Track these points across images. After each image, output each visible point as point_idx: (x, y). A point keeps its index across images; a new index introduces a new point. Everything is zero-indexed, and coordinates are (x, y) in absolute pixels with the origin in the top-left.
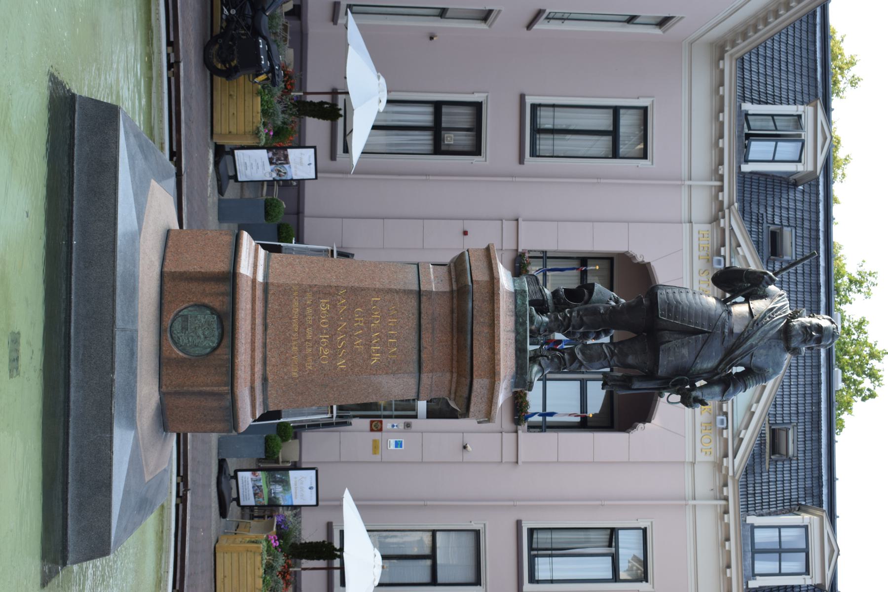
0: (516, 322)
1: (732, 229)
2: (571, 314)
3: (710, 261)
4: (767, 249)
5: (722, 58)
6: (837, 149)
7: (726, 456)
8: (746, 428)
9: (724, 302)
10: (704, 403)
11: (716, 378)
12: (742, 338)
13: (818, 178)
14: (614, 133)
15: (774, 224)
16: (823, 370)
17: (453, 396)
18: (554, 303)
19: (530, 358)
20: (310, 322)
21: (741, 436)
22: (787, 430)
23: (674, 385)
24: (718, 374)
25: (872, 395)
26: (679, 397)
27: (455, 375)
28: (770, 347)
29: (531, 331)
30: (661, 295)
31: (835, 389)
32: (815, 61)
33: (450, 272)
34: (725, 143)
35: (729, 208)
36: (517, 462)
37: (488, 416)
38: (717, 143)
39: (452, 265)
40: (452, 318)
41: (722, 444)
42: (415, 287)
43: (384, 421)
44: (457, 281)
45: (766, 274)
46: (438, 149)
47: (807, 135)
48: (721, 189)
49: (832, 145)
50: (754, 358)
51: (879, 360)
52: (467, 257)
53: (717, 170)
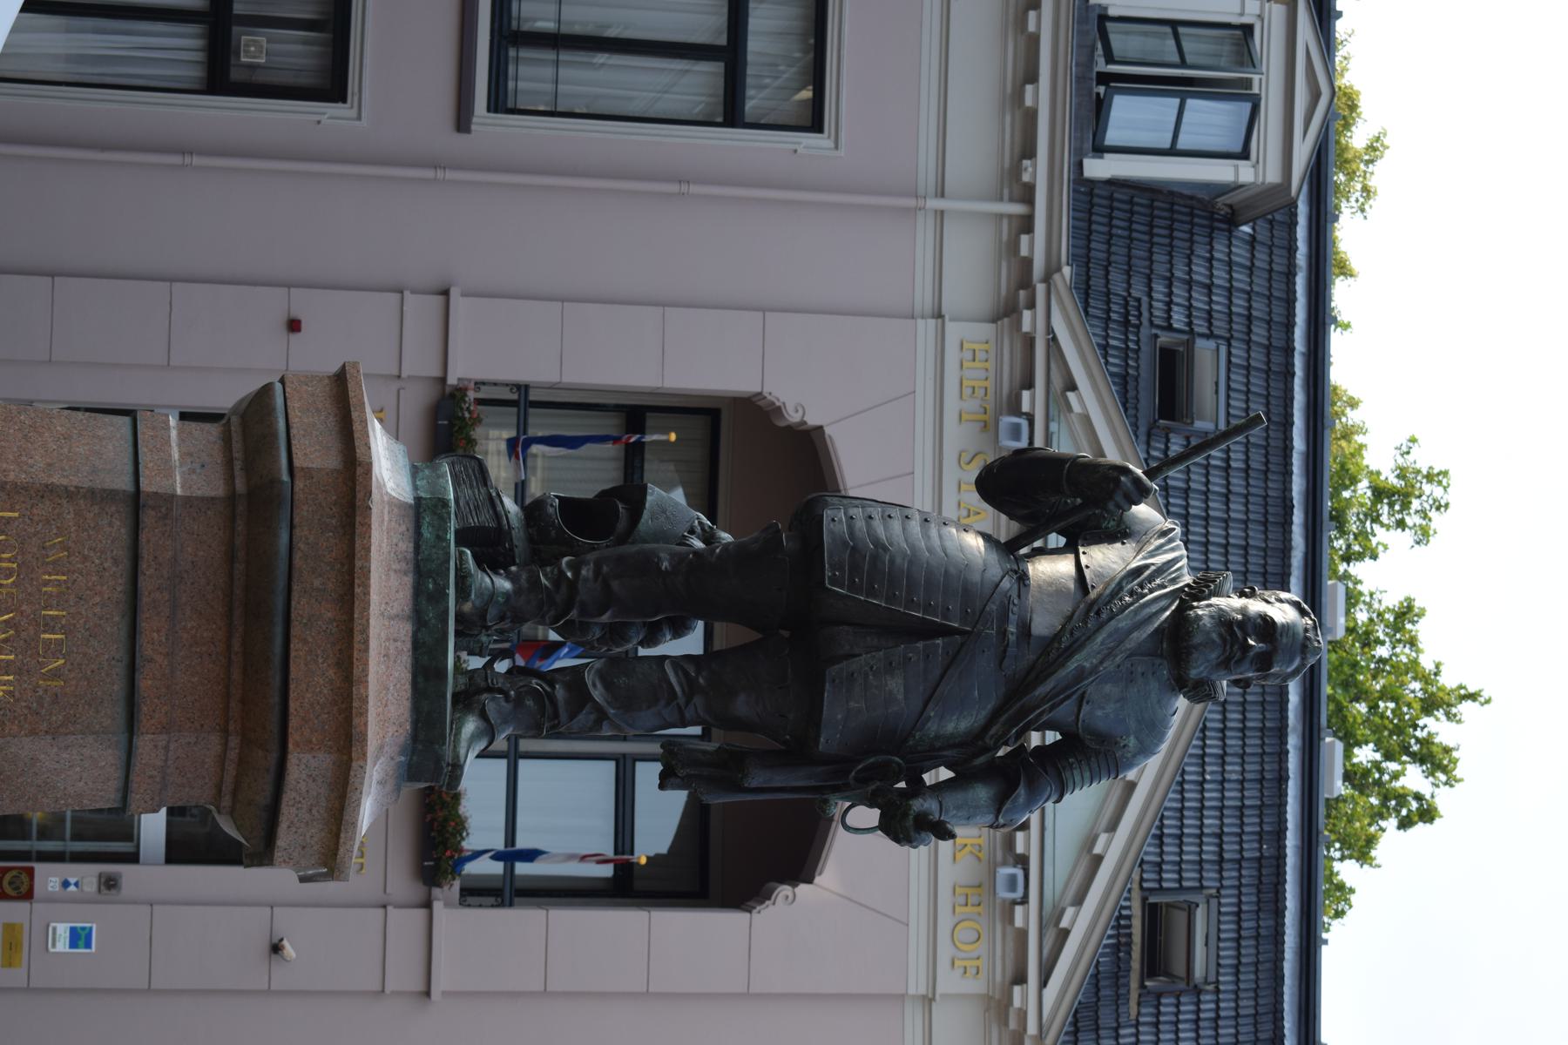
0: (418, 591)
1: (1053, 340)
2: (577, 573)
3: (989, 427)
4: (1148, 398)
6: (1347, 126)
7: (1020, 979)
8: (1079, 901)
9: (1008, 549)
10: (944, 833)
11: (981, 760)
12: (1057, 648)
13: (1293, 205)
14: (730, 53)
15: (1170, 328)
16: (1293, 742)
17: (226, 801)
18: (530, 540)
19: (455, 695)
21: (1064, 924)
22: (1190, 909)
23: (863, 780)
24: (986, 750)
25: (1428, 814)
26: (876, 812)
27: (234, 741)
28: (1130, 678)
29: (459, 617)
30: (834, 521)
31: (1325, 794)
33: (227, 439)
34: (1041, 96)
35: (1047, 279)
36: (428, 994)
37: (329, 860)
38: (1019, 95)
39: (235, 420)
40: (231, 576)
41: (1010, 945)
42: (124, 483)
43: (40, 868)
44: (249, 468)
45: (1126, 471)
46: (220, 76)
47: (1268, 82)
48: (1026, 224)
49: (1338, 110)
50: (1086, 708)
51: (1450, 717)
52: (279, 401)
53: (1016, 171)
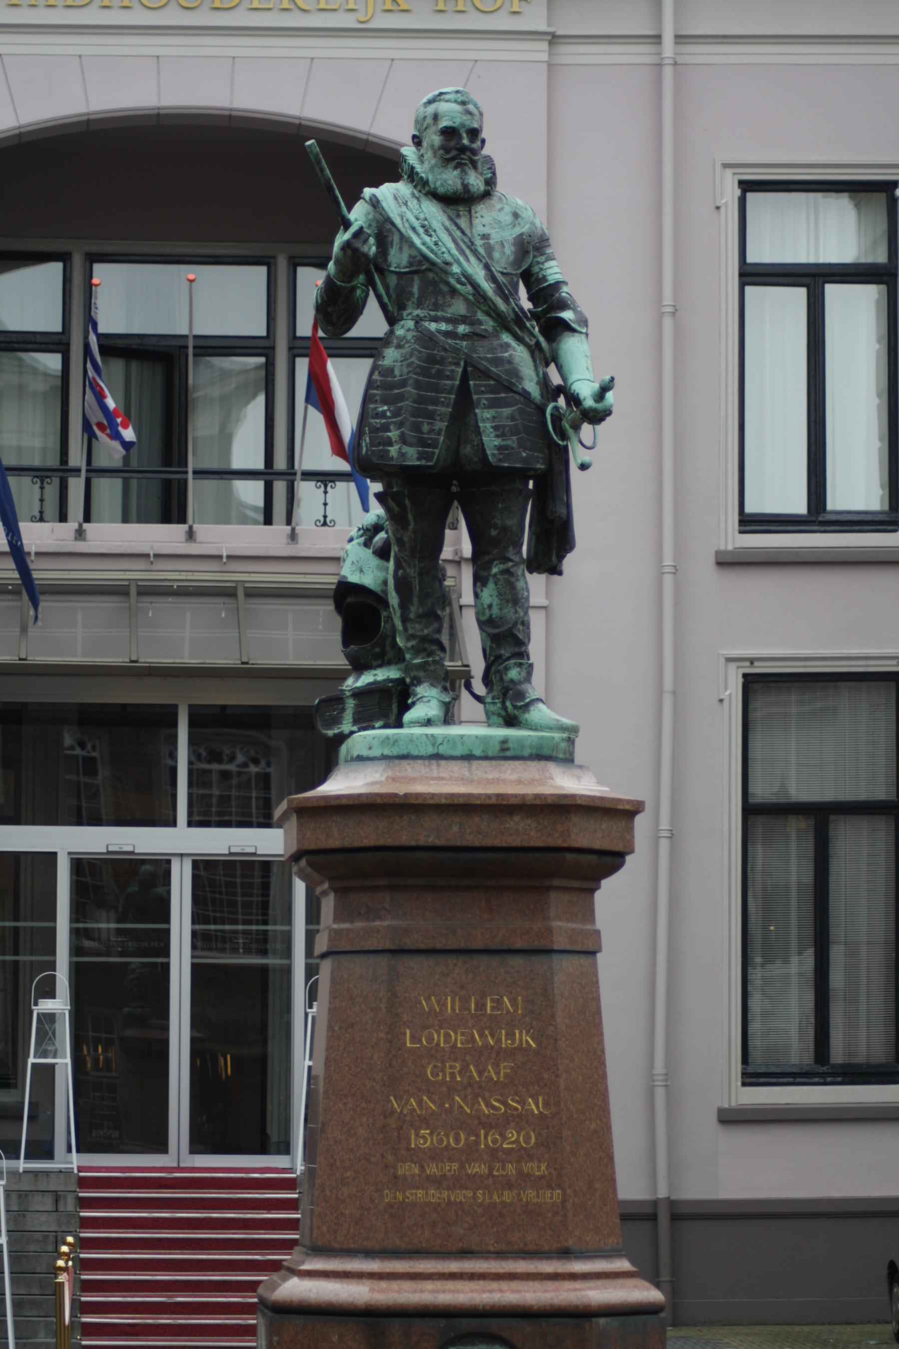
20: (455, 1166)
27: (556, 882)
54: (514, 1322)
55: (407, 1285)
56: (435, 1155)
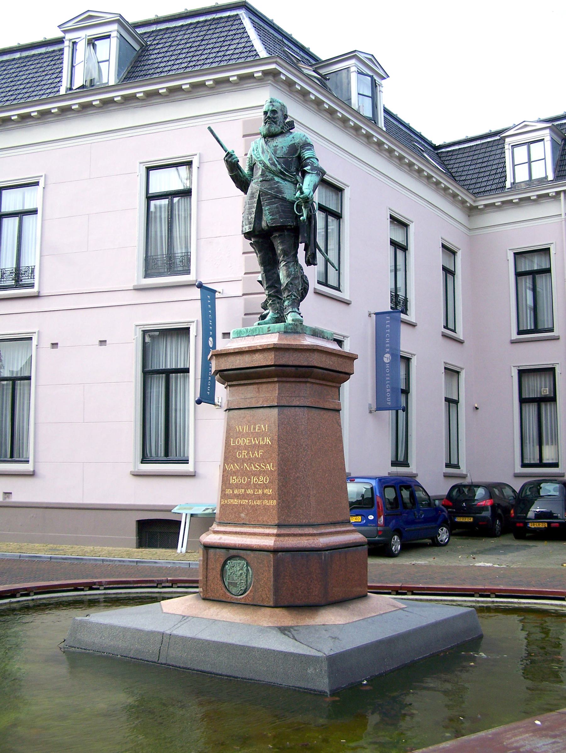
5: (477, 207)
14: (533, 273)
20: (243, 490)
32: (483, 144)
46: (552, 399)
54: (248, 552)
55: (291, 538)
56: (238, 486)
